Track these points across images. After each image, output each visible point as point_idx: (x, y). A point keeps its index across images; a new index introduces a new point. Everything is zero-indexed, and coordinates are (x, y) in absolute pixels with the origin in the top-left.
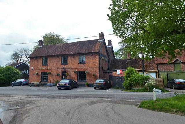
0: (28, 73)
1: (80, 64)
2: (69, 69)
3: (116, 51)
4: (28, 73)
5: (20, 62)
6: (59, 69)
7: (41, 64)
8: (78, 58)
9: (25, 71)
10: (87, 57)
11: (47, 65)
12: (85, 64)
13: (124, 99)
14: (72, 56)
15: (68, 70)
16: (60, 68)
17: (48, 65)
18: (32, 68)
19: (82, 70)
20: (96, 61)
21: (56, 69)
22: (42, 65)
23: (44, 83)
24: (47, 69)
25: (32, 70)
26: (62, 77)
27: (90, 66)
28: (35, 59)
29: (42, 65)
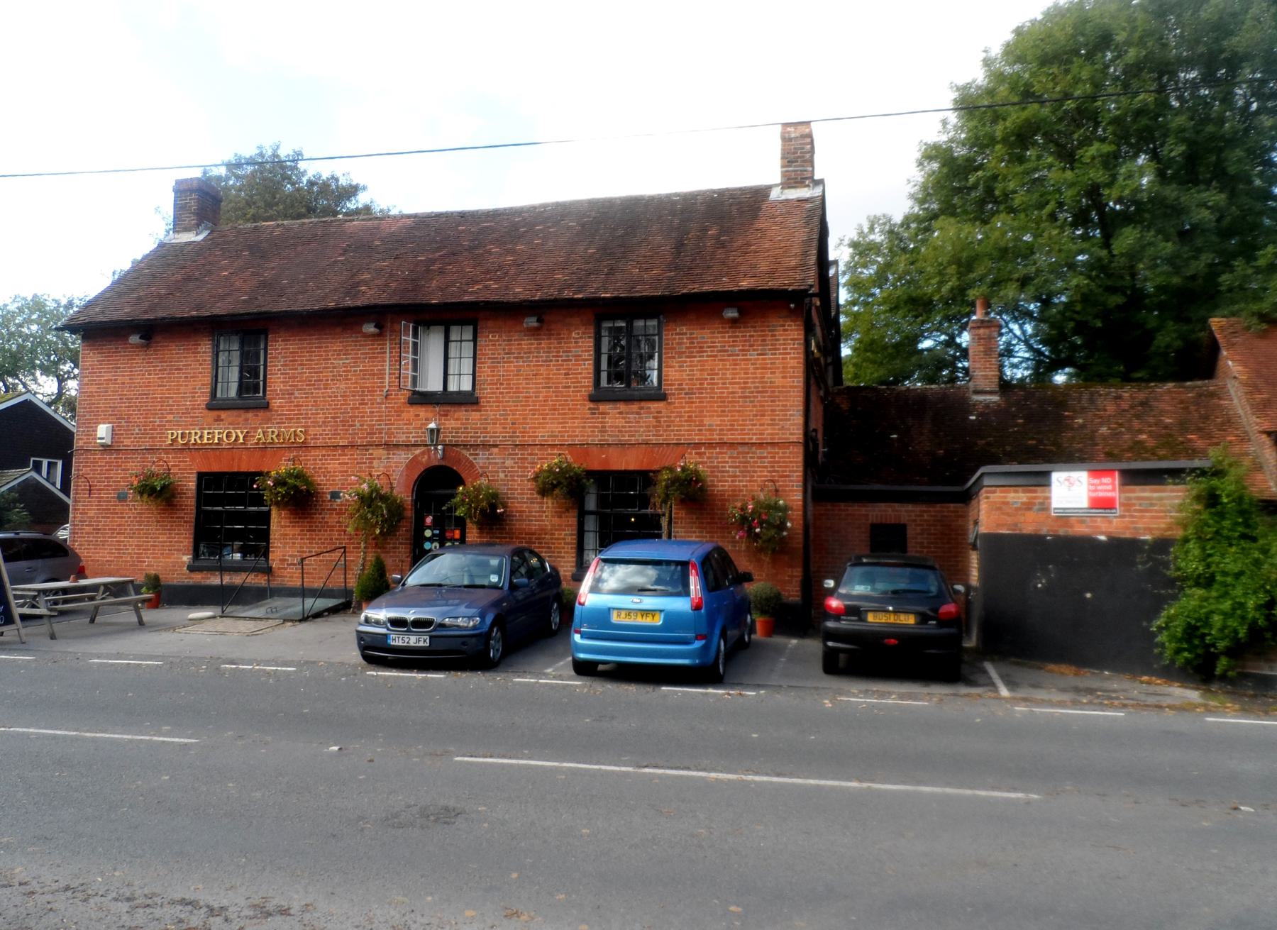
0: (65, 488)
1: (604, 407)
2: (486, 446)
3: (344, 184)
4: (65, 488)
5: (221, 348)
6: (388, 446)
7: (204, 398)
8: (590, 343)
9: (37, 467)
10: (493, 342)
11: (267, 407)
12: (654, 406)
13: (1151, 700)
14: (370, 328)
15: (480, 459)
16: (402, 438)
17: (276, 403)
18: (103, 431)
19: (629, 462)
20: (778, 380)
21: (353, 446)
22: (210, 407)
23: (227, 579)
24: (263, 448)
25: (106, 448)
26: (420, 527)
27: (714, 423)
28: (135, 339)
29: (210, 407)
